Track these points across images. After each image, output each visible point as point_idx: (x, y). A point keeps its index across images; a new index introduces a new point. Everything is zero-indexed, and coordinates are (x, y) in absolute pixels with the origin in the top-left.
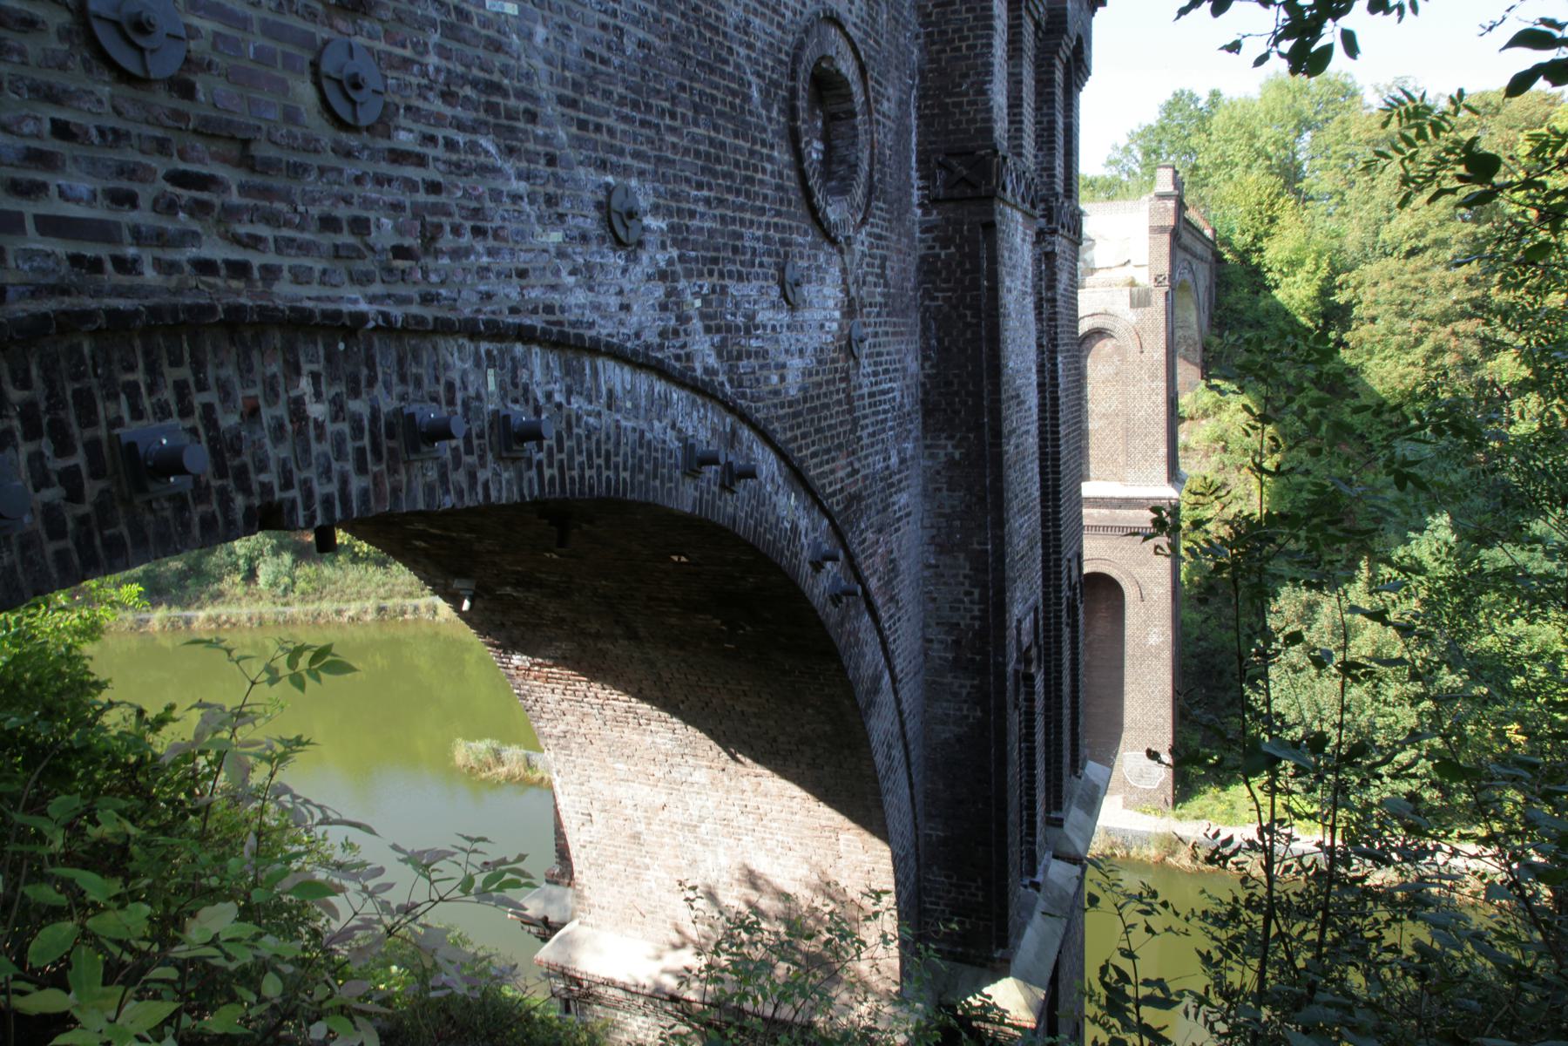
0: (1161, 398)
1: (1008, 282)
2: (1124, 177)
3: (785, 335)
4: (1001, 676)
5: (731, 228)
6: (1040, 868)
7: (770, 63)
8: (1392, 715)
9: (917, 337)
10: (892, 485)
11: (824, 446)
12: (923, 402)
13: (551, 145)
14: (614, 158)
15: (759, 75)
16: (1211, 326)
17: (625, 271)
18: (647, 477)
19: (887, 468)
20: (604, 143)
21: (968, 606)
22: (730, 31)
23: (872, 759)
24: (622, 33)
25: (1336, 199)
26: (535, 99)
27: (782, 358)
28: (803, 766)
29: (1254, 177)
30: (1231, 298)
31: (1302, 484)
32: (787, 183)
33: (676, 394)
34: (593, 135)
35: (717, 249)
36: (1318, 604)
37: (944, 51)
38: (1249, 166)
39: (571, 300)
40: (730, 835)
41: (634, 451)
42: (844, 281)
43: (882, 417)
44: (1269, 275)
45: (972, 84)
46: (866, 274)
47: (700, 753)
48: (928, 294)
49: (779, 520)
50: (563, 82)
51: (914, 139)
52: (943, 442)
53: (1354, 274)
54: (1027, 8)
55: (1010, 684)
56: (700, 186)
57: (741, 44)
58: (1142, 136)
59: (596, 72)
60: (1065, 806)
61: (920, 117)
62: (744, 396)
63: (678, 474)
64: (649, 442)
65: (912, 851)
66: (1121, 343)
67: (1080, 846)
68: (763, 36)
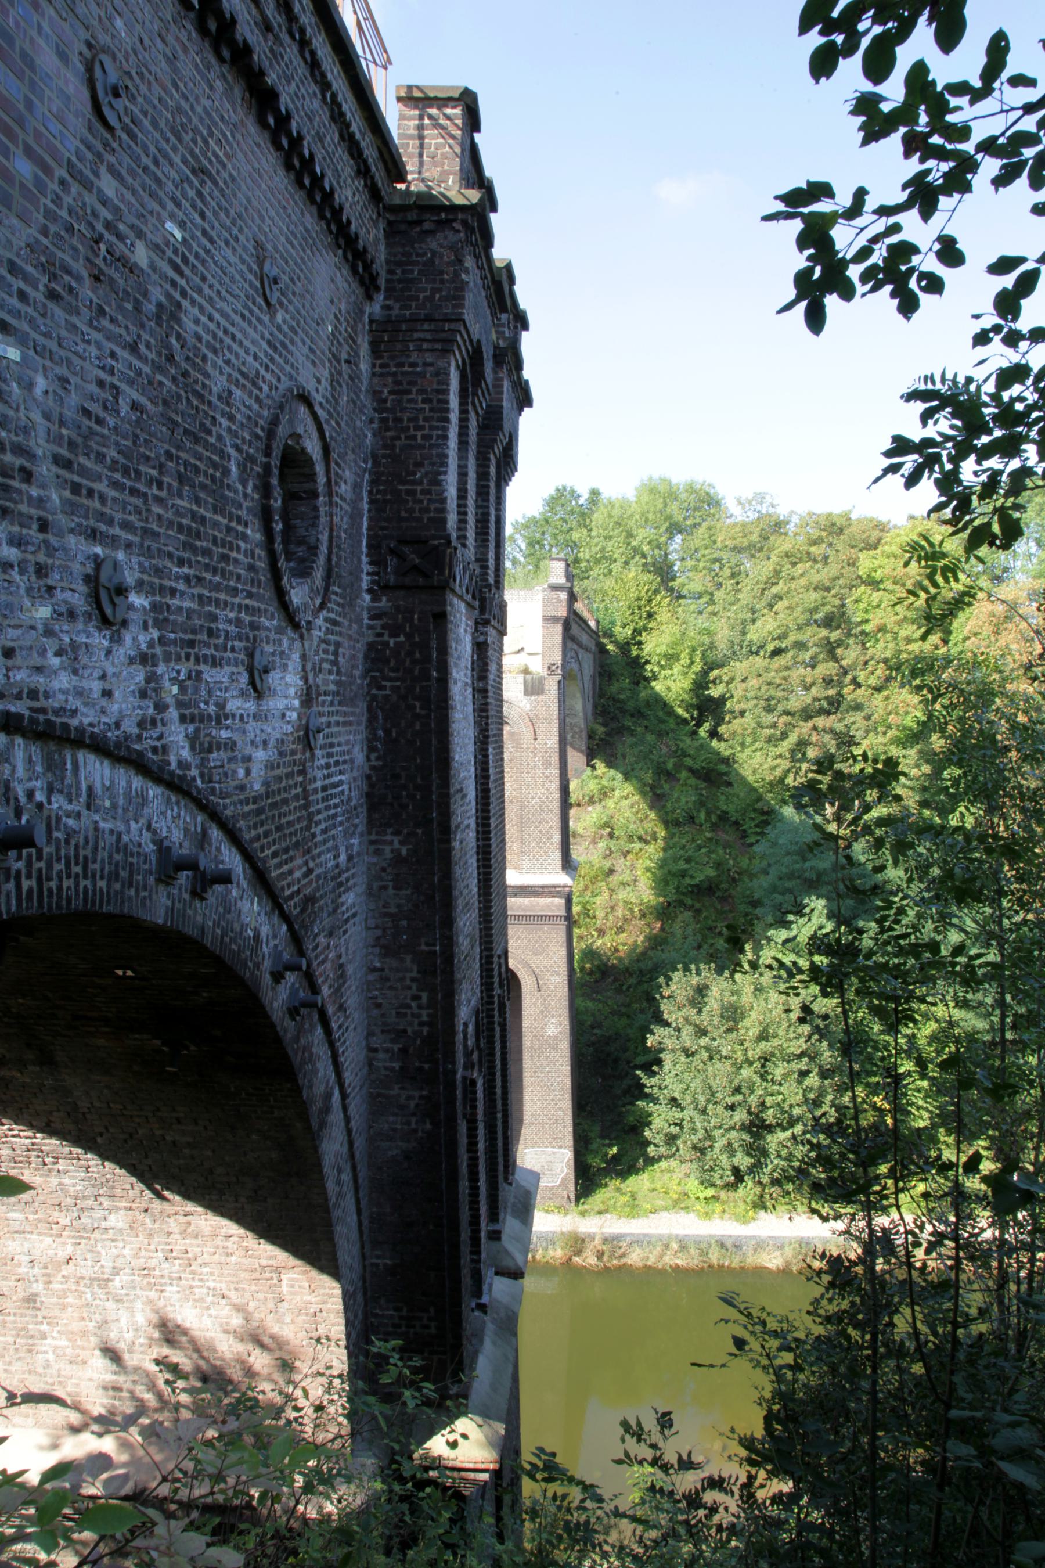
0: (555, 786)
3: (251, 726)
4: (451, 1085)
5: (207, 608)
6: (485, 1288)
7: (248, 437)
8: (780, 1093)
9: (363, 727)
10: (340, 885)
11: (284, 845)
12: (368, 795)
13: (44, 509)
14: (103, 527)
15: (238, 450)
17: (109, 652)
18: (123, 886)
19: (337, 866)
20: (95, 511)
21: (416, 1011)
22: (214, 400)
23: (323, 1187)
24: (118, 393)
25: (705, 599)
26: (31, 456)
27: (248, 750)
28: (243, 1200)
29: (633, 574)
30: (614, 688)
31: (686, 870)
32: (258, 564)
33: (154, 791)
34: (85, 501)
35: (194, 632)
36: (707, 987)
37: (399, 438)
38: (626, 563)
39: (56, 685)
40: (151, 1286)
41: (111, 857)
42: (304, 669)
43: (333, 811)
44: (648, 667)
45: (427, 474)
46: (322, 660)
47: (118, 1192)
48: (375, 683)
49: (244, 927)
50: (59, 439)
51: (365, 524)
52: (389, 838)
53: (726, 670)
54: (473, 404)
55: (459, 1092)
56: (181, 562)
57: (223, 415)
58: (526, 527)
59: (92, 433)
60: (501, 1216)
61: (371, 502)
62: (213, 791)
63: (152, 880)
64: (126, 845)
65: (360, 1284)
66: (515, 729)
67: (519, 1258)
68: (243, 409)
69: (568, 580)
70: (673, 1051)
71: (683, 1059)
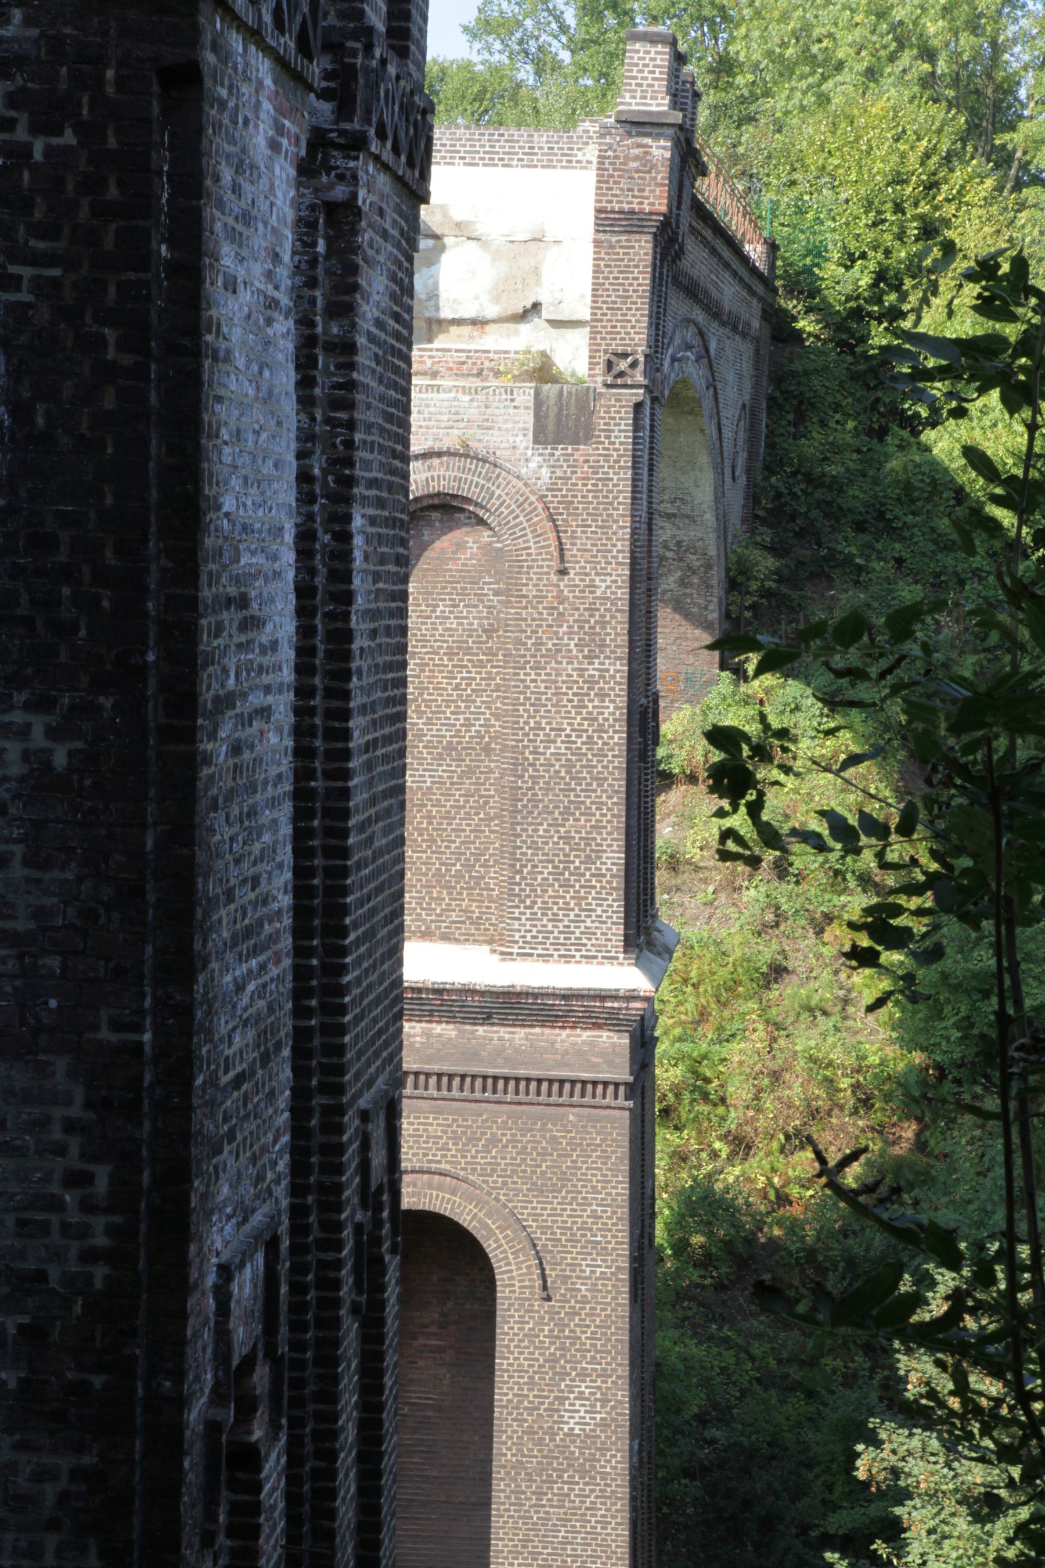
1: (227, 259)
2: (526, 73)
16: (753, 519)
21: (75, 1217)
38: (872, 74)
66: (506, 542)
69: (675, 105)
70: (933, 1496)
71: (962, 1524)
